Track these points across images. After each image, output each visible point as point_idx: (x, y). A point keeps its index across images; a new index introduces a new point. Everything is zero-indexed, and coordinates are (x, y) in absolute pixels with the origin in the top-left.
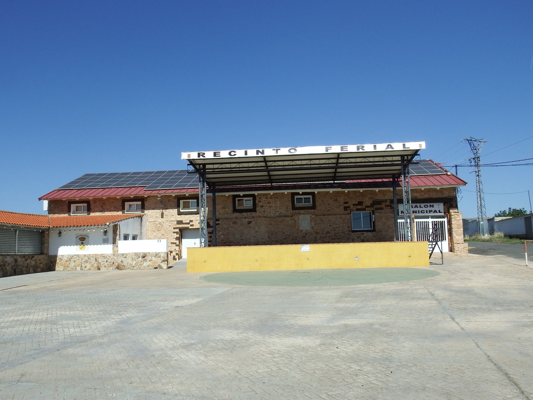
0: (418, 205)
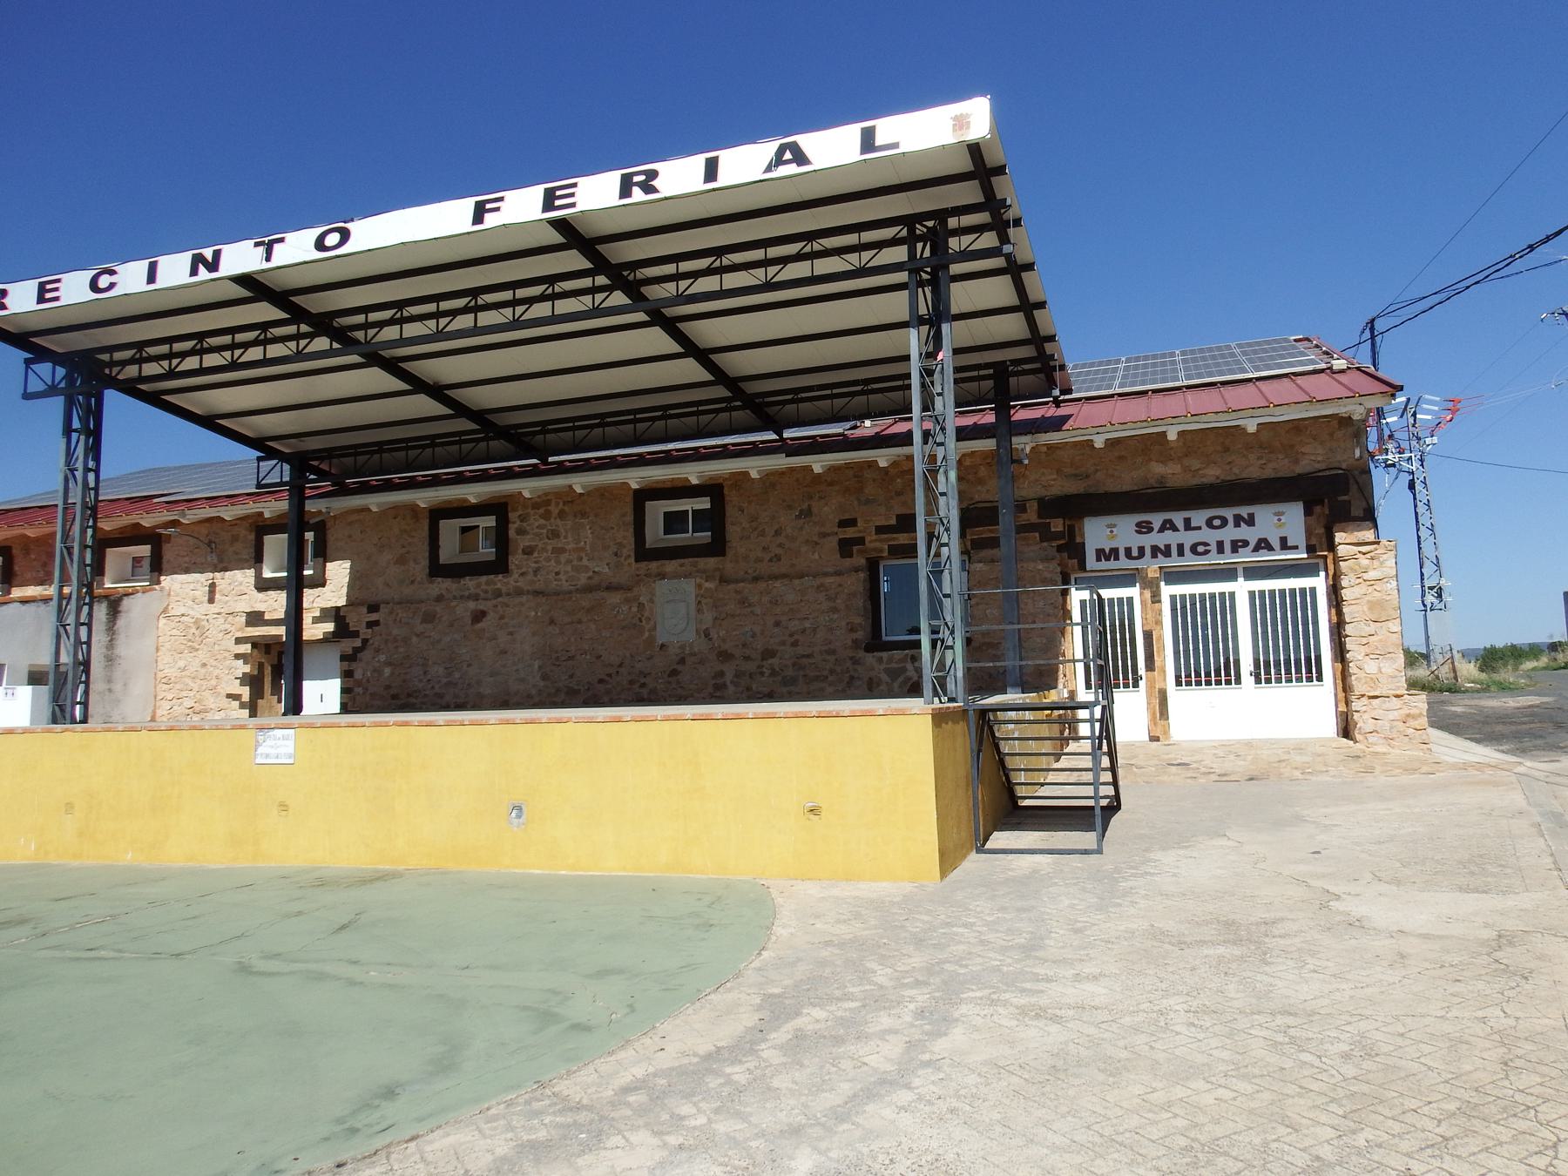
0: (1178, 518)
